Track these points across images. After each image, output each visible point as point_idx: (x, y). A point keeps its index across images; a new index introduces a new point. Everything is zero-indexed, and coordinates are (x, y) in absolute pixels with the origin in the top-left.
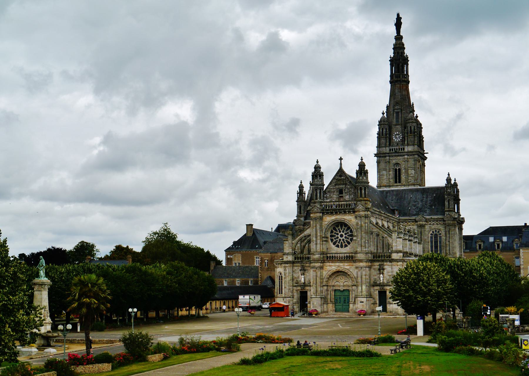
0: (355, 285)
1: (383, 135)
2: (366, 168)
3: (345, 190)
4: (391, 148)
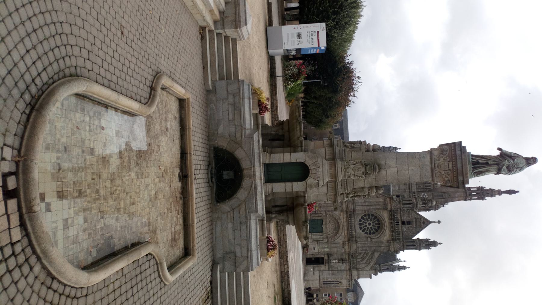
0: (328, 241)
1: (426, 186)
2: (433, 248)
3: (411, 227)
4: (416, 193)
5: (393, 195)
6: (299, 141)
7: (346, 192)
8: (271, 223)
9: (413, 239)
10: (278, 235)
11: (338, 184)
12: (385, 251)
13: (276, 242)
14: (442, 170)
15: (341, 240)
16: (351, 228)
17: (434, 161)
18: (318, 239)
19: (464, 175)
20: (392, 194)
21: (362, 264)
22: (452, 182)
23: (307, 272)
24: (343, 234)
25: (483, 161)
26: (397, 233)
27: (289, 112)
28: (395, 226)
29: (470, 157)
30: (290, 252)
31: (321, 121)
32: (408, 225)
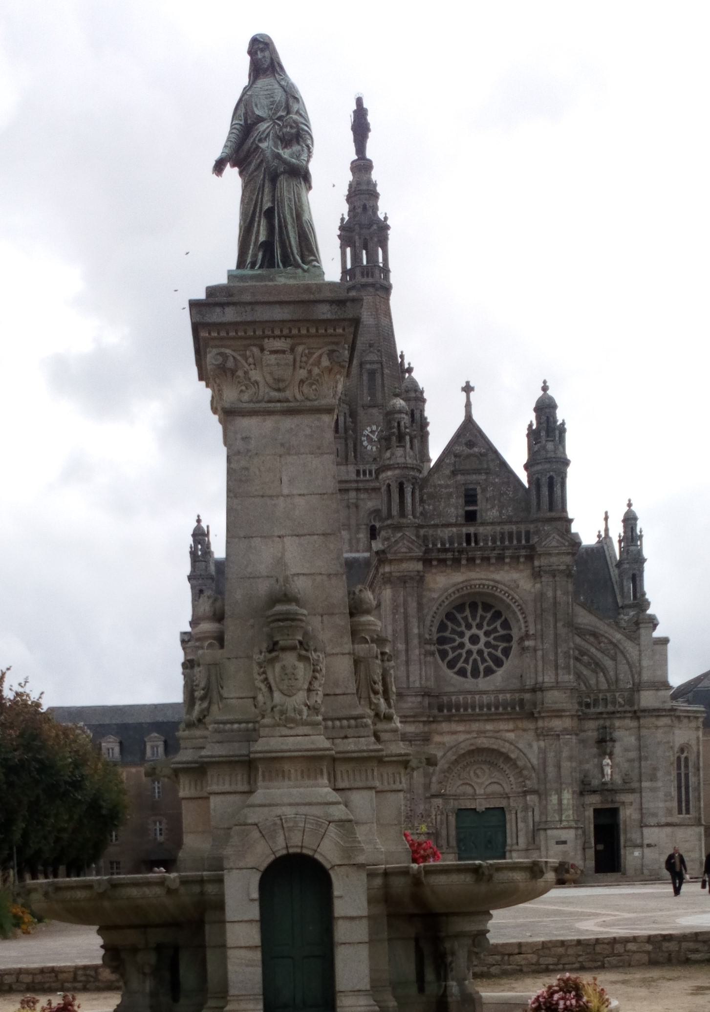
2: (561, 415)
3: (484, 490)
4: (361, 468)
5: (369, 549)
6: (182, 890)
7: (369, 721)
8: (481, 997)
9: (527, 485)
10: (519, 972)
11: (341, 749)
12: (571, 588)
13: (553, 980)
14: (293, 375)
15: (530, 746)
17: (259, 402)
18: (527, 826)
19: (312, 297)
20: (367, 555)
21: (616, 669)
22: (337, 344)
23: (646, 872)
24: (511, 736)
25: (261, 228)
26: (507, 543)
27: (78, 927)
28: (481, 549)
29: (248, 272)
30: (579, 931)
31: (94, 806)
32: (479, 502)
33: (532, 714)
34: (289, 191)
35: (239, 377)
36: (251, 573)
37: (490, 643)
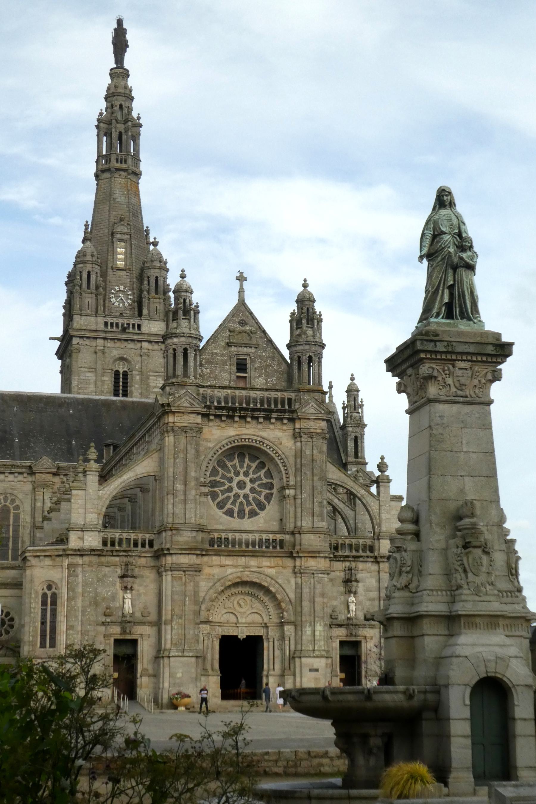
1: (89, 287)
3: (252, 361)
4: (110, 320)
15: (289, 582)
16: (254, 545)
24: (272, 572)
32: (248, 371)
33: (291, 553)
34: (467, 278)
35: (439, 381)
36: (445, 497)
37: (255, 489)
